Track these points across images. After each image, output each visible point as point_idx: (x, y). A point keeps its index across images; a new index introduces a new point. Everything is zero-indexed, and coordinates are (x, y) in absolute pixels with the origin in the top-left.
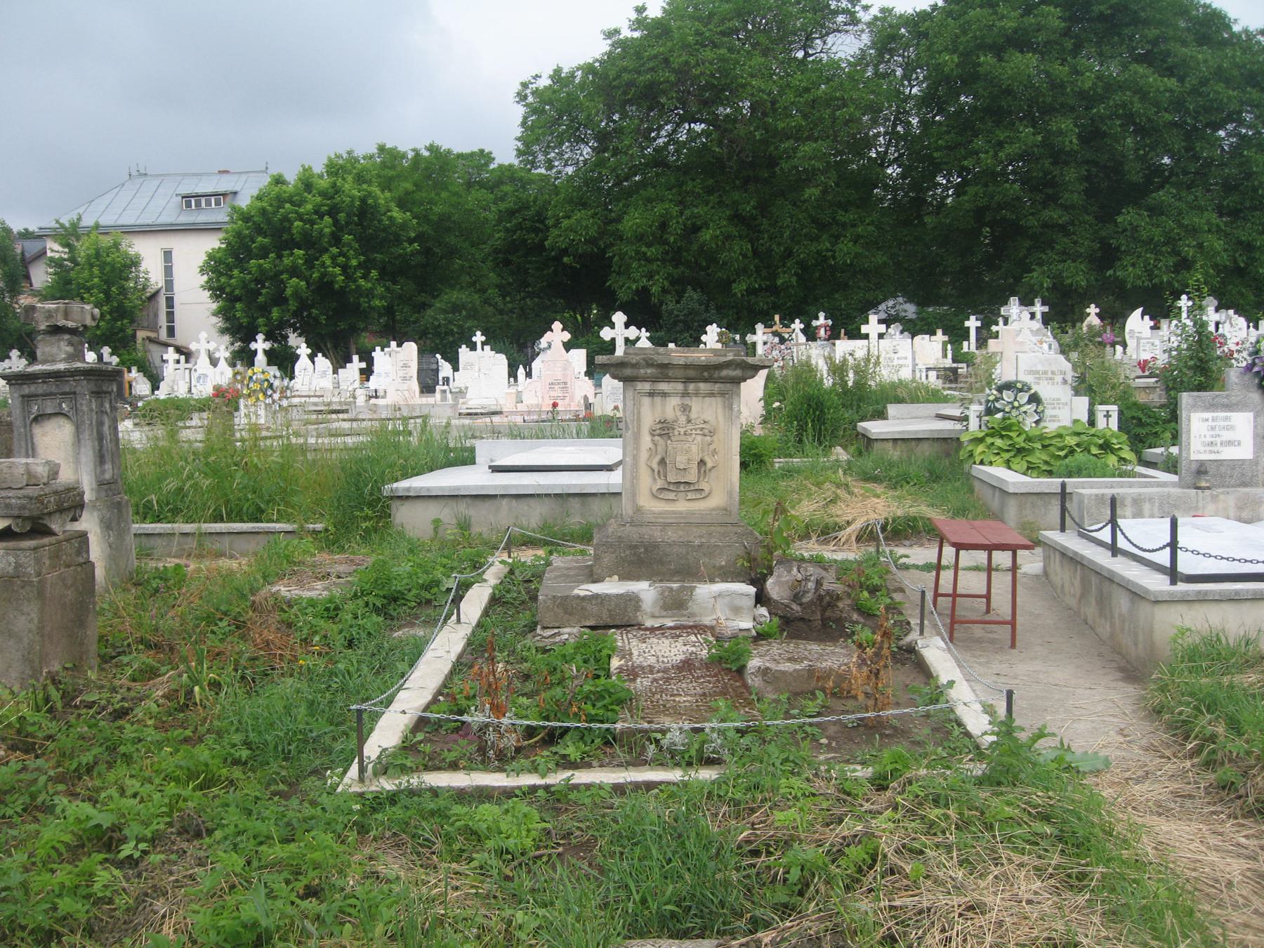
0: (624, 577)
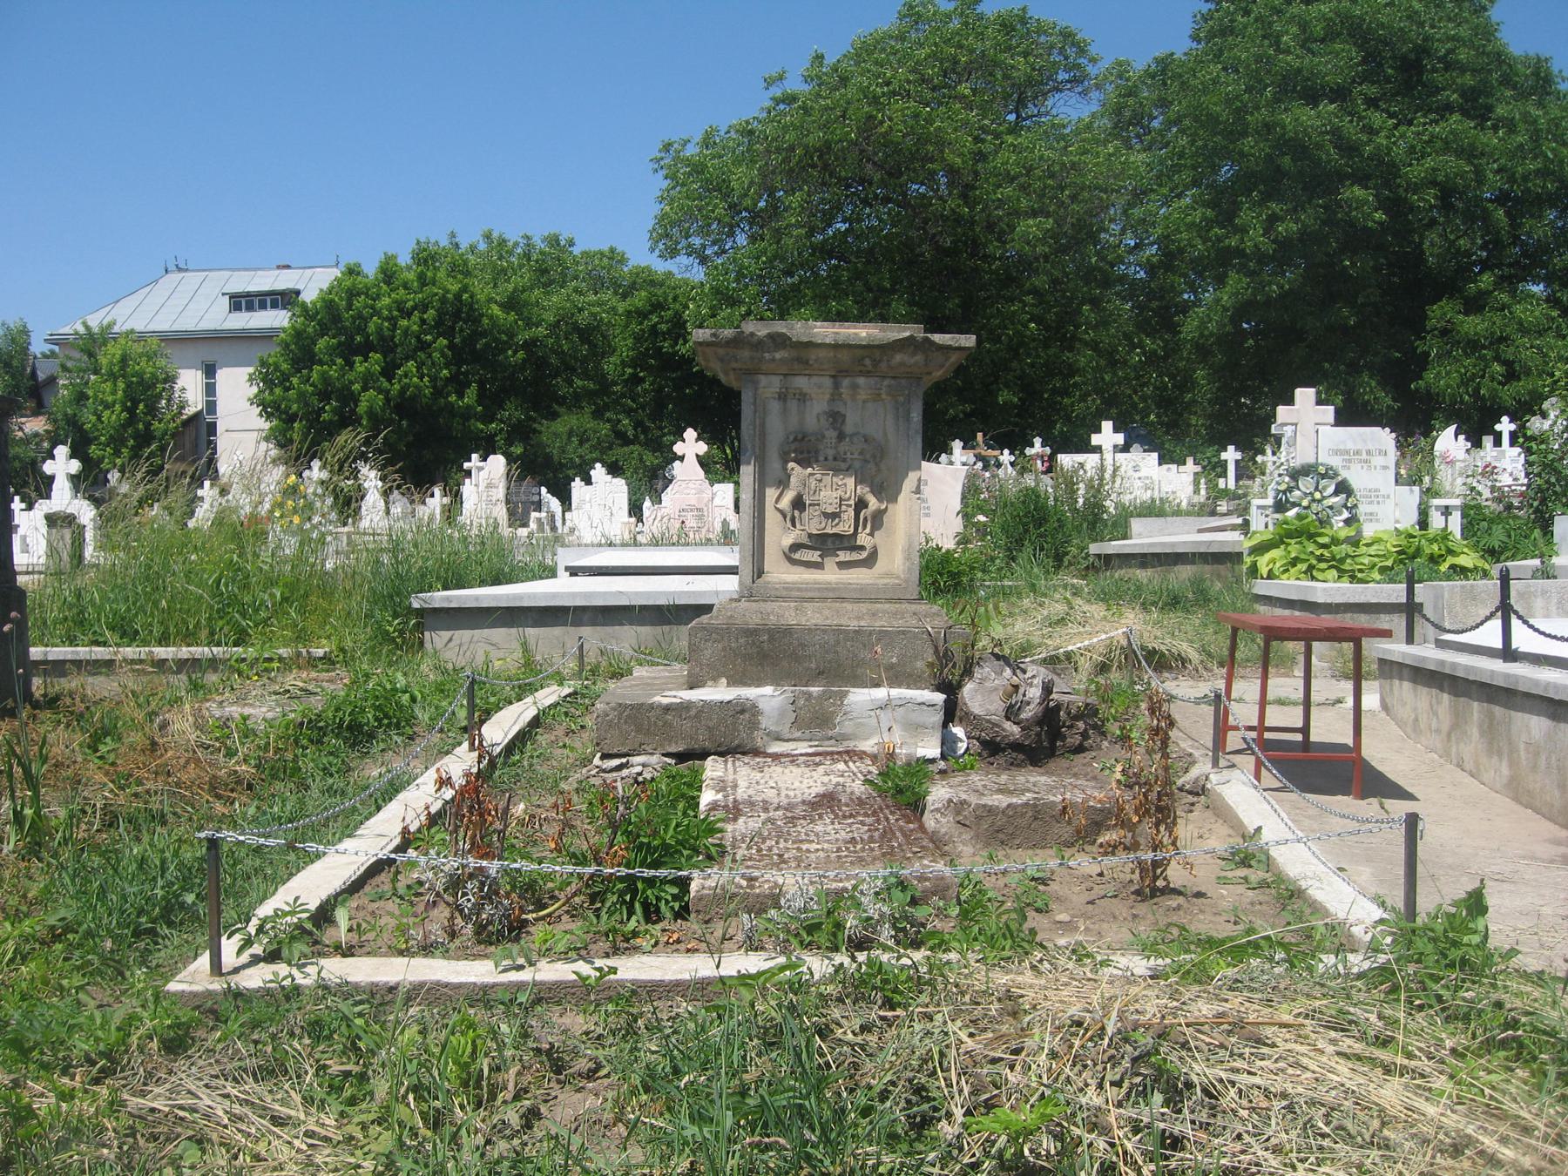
0: (734, 682)
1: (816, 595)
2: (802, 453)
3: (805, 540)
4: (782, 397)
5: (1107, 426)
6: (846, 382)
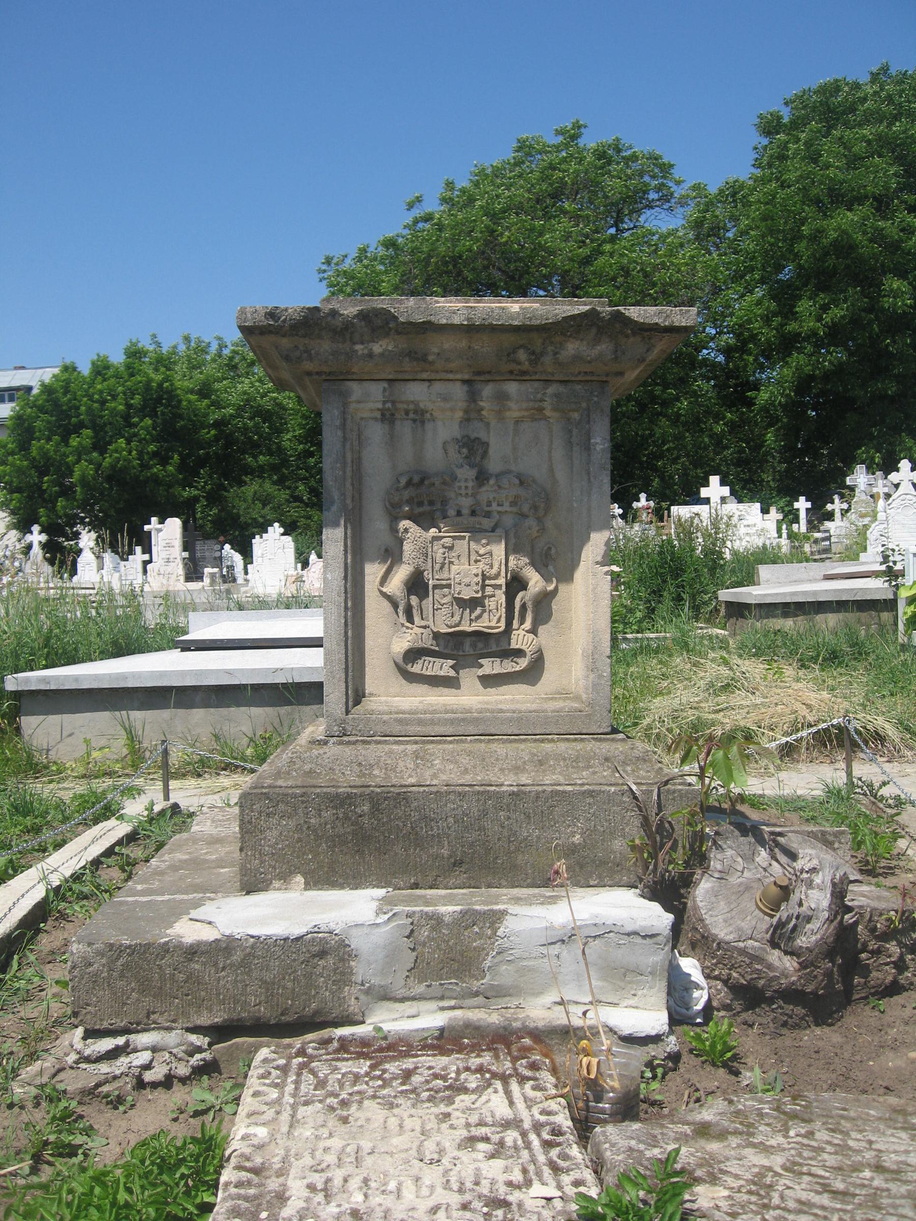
1: (449, 730)
2: (420, 504)
3: (429, 643)
4: (388, 417)
5: (714, 480)
6: (488, 390)
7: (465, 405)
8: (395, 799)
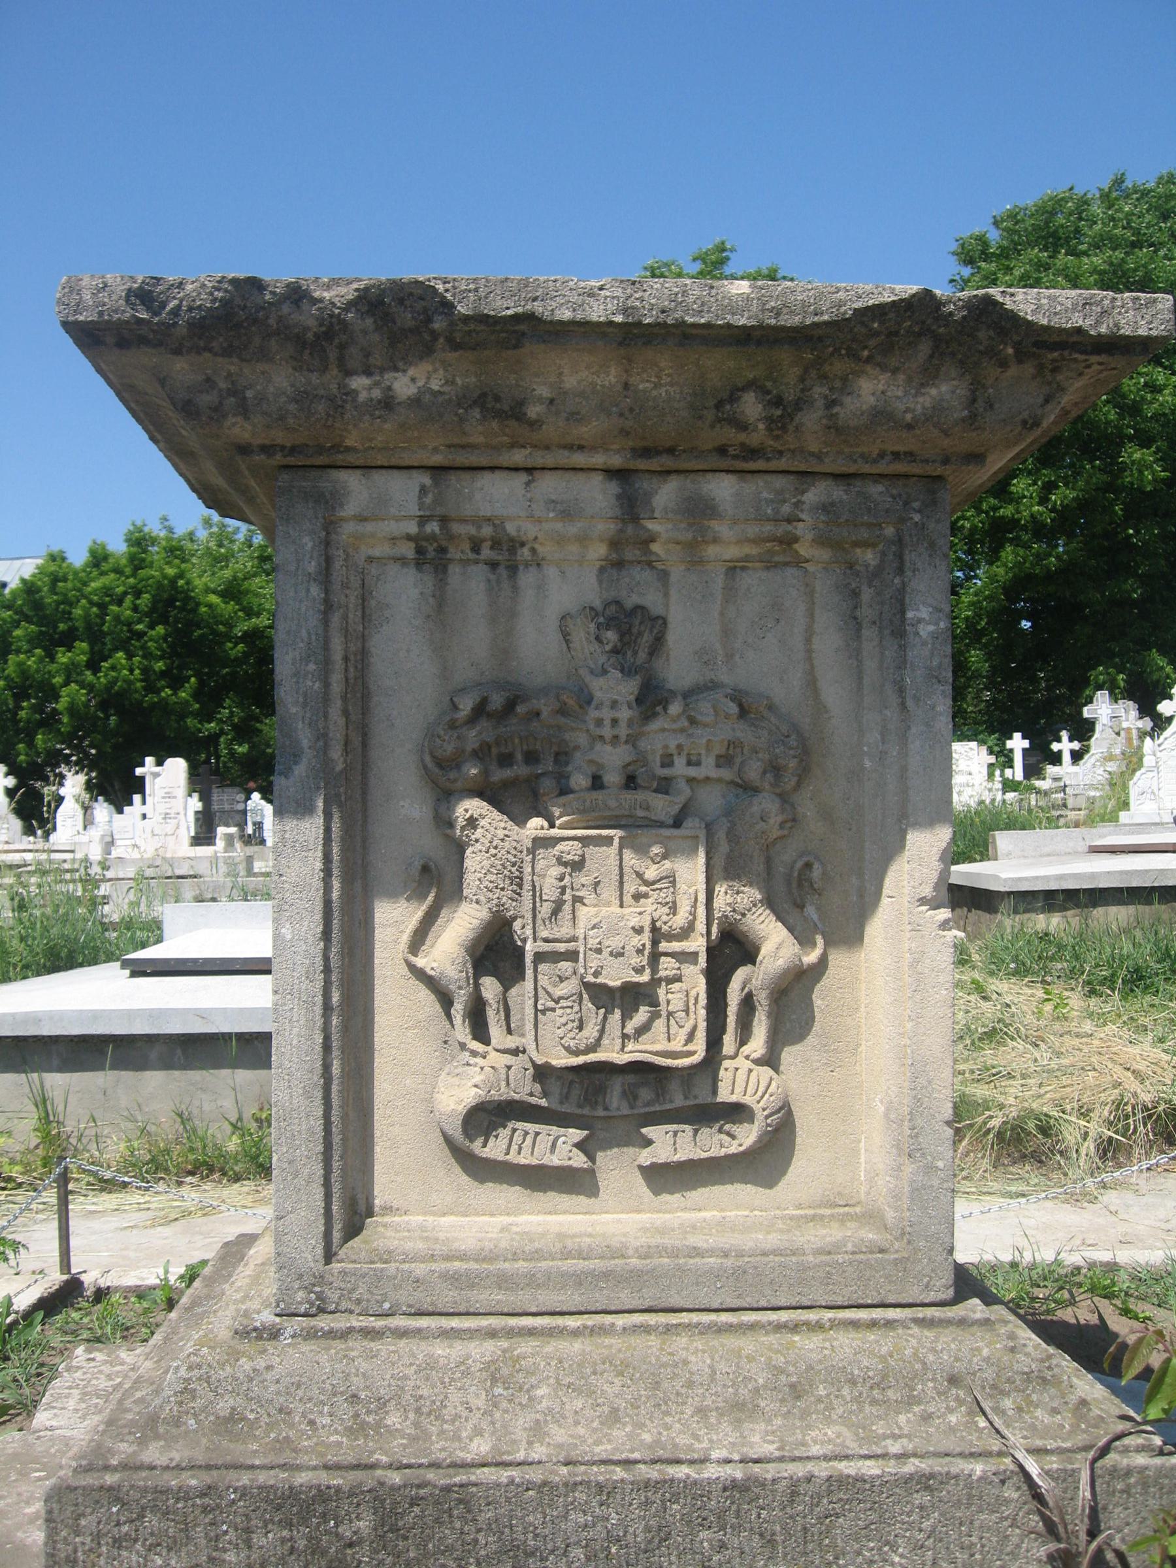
2: (506, 760)
3: (525, 1090)
7: (612, 527)
8: (437, 1503)
